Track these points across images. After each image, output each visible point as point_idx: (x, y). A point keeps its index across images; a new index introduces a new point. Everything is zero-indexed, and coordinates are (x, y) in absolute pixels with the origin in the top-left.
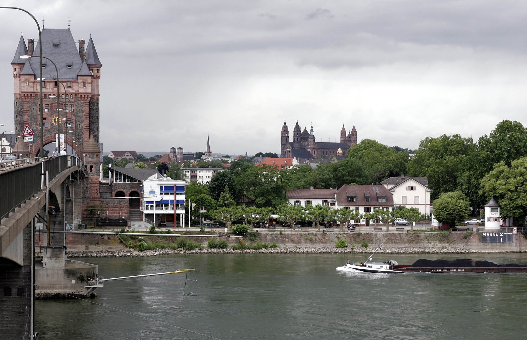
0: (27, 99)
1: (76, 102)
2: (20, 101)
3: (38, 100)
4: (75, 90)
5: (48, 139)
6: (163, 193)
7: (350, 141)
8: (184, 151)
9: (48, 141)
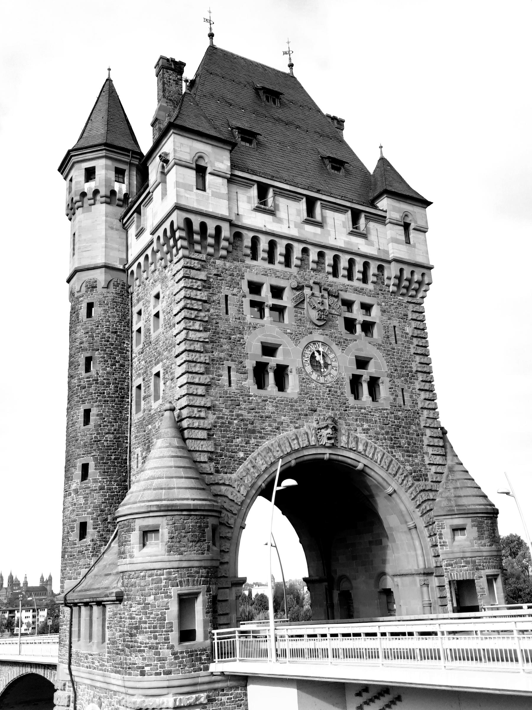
0: (198, 247)
1: (381, 297)
2: (110, 296)
3: (244, 261)
4: (376, 246)
5: (296, 447)
6: (302, 651)
7: (47, 585)
8: (29, 585)
9: (295, 456)
